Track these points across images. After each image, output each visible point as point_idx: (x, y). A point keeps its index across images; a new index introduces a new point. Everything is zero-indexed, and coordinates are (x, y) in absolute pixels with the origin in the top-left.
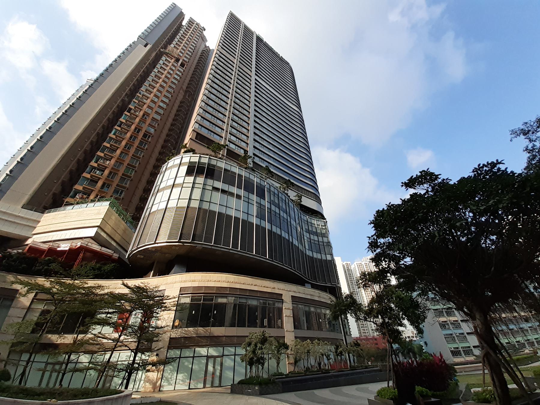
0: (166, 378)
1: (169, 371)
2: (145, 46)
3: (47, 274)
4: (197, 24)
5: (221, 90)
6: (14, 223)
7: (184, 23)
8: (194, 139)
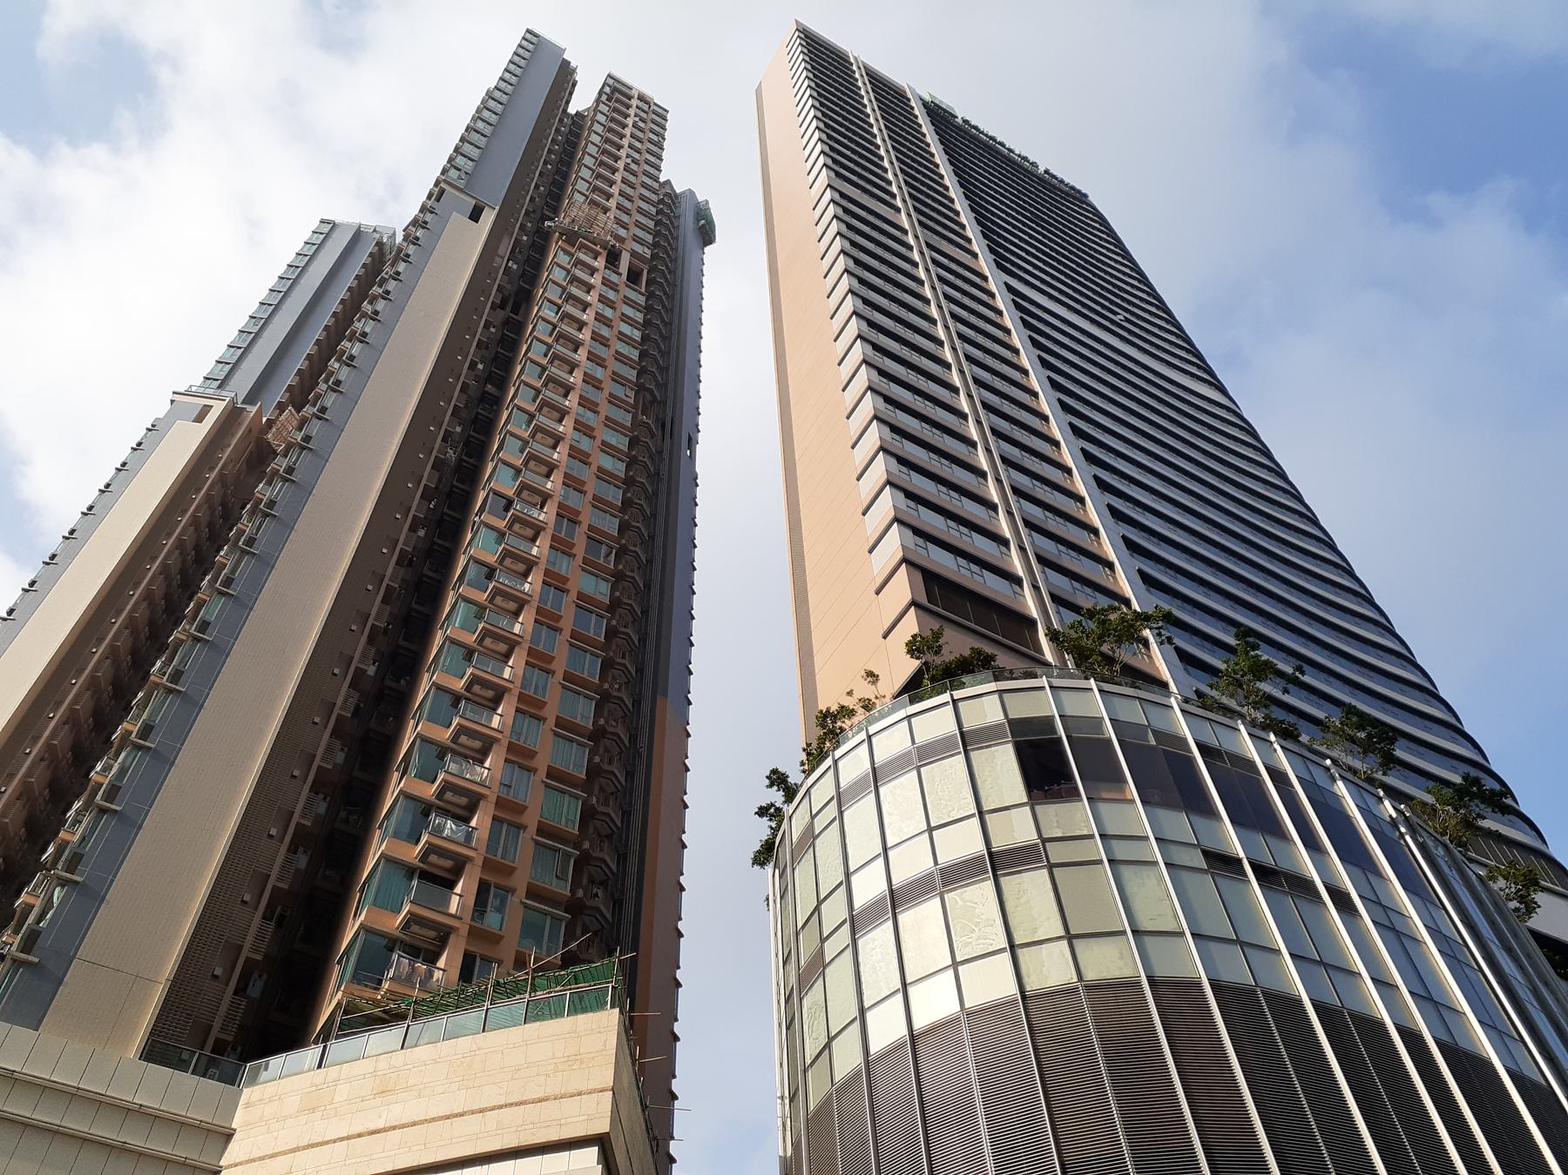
2: (475, 216)
3: (1282, 725)
4: (641, 98)
6: (122, 1150)
7: (581, 100)
8: (924, 600)
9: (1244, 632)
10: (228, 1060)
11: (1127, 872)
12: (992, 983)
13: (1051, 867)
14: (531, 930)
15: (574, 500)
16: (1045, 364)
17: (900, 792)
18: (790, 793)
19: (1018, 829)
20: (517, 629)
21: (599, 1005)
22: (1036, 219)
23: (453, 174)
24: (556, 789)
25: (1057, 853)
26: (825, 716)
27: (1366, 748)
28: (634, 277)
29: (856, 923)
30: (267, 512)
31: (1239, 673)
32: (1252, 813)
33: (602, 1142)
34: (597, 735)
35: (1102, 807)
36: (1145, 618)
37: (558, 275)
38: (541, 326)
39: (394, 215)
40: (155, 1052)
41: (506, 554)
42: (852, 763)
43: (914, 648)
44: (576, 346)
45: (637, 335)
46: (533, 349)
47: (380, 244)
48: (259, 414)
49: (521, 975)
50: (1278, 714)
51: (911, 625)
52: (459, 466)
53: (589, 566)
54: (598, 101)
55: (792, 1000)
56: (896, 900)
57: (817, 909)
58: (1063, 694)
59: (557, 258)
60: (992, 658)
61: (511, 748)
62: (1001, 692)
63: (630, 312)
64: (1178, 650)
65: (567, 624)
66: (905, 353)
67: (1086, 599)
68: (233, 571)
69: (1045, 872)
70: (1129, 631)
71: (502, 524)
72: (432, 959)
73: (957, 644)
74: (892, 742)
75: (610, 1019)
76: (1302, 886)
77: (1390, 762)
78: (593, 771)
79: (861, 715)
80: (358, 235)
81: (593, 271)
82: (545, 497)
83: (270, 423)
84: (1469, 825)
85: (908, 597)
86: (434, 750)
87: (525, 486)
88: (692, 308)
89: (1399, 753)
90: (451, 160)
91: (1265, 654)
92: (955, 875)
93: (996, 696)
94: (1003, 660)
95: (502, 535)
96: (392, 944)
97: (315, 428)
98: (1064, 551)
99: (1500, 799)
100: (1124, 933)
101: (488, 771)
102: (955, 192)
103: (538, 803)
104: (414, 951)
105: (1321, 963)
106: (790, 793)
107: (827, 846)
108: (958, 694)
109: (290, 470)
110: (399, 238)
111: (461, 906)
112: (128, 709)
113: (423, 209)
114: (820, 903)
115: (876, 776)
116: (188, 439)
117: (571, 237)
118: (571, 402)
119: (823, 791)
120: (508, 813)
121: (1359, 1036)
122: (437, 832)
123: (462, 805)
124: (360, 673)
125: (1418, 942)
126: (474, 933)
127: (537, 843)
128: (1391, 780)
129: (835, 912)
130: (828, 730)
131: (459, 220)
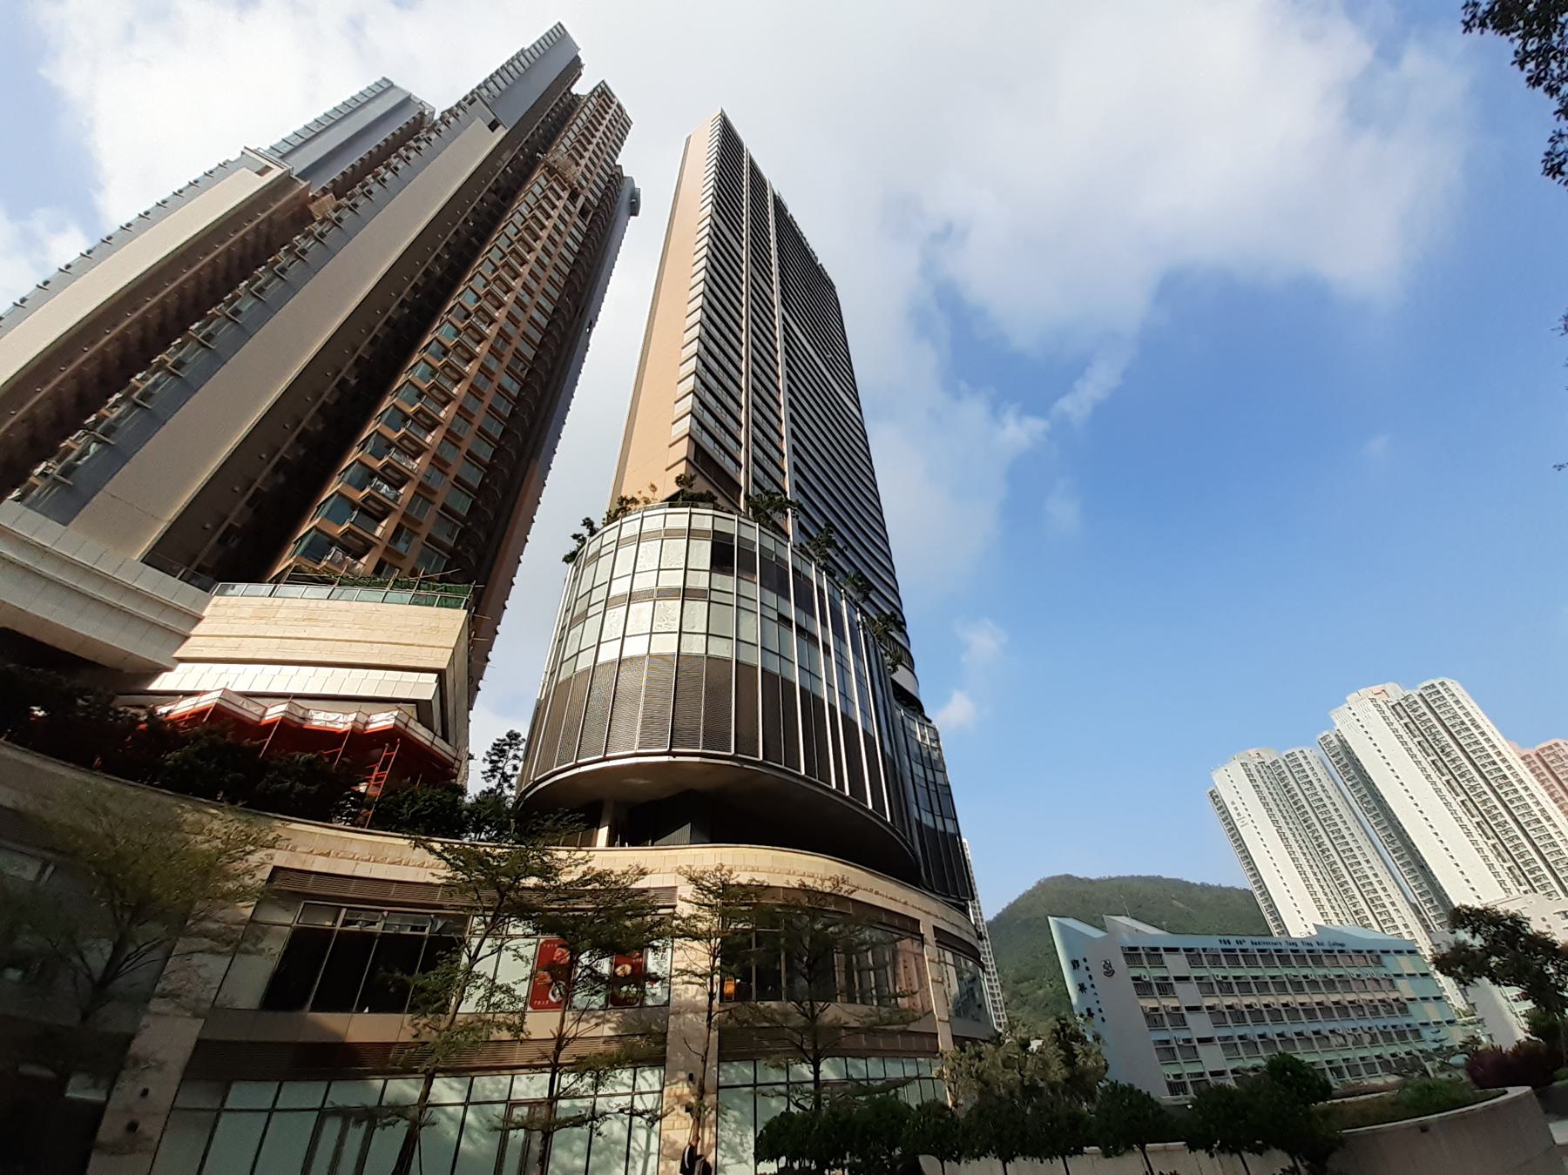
0: (728, 1145)
1: (733, 1126)
2: (493, 126)
4: (619, 106)
5: (726, 331)
6: (120, 610)
7: (582, 88)
9: (829, 524)
10: (206, 579)
11: (743, 613)
12: (666, 645)
14: (424, 558)
15: (510, 329)
16: (788, 364)
17: (650, 549)
18: (593, 532)
19: (700, 581)
20: (455, 391)
21: (458, 607)
23: (484, 91)
25: (715, 596)
26: (623, 499)
27: (859, 590)
28: (583, 213)
29: (608, 603)
31: (819, 543)
32: (805, 604)
33: (441, 674)
34: (490, 467)
36: (790, 502)
38: (517, 216)
39: (439, 96)
40: (151, 559)
41: (458, 344)
42: (630, 527)
43: (679, 481)
44: (536, 238)
46: (511, 226)
47: (422, 114)
48: (308, 188)
49: (412, 579)
50: (830, 564)
51: (681, 469)
52: (440, 280)
53: (509, 371)
54: (592, 93)
55: (565, 630)
56: (631, 597)
59: (538, 181)
61: (435, 457)
65: (487, 400)
66: (721, 357)
67: (768, 485)
68: (267, 284)
70: (782, 507)
71: (461, 326)
72: (358, 557)
73: (700, 486)
74: (654, 522)
75: (462, 614)
76: (814, 639)
77: (866, 598)
79: (642, 505)
80: (408, 100)
81: (559, 198)
82: (493, 321)
83: (314, 198)
84: (886, 631)
86: (385, 443)
87: (480, 309)
88: (613, 247)
90: (486, 82)
91: (834, 536)
92: (665, 594)
94: (720, 501)
96: (332, 541)
97: (347, 215)
98: (765, 461)
99: (901, 625)
101: (416, 465)
103: (444, 491)
104: (347, 550)
106: (593, 532)
107: (605, 563)
109: (322, 235)
110: (437, 117)
111: (384, 533)
112: (168, 346)
113: (458, 105)
115: (640, 538)
116: (247, 185)
117: (551, 171)
118: (524, 270)
119: (611, 536)
120: (424, 492)
121: (812, 703)
122: (377, 488)
123: (397, 479)
124: (343, 382)
128: (864, 606)
129: (598, 595)
130: (622, 507)
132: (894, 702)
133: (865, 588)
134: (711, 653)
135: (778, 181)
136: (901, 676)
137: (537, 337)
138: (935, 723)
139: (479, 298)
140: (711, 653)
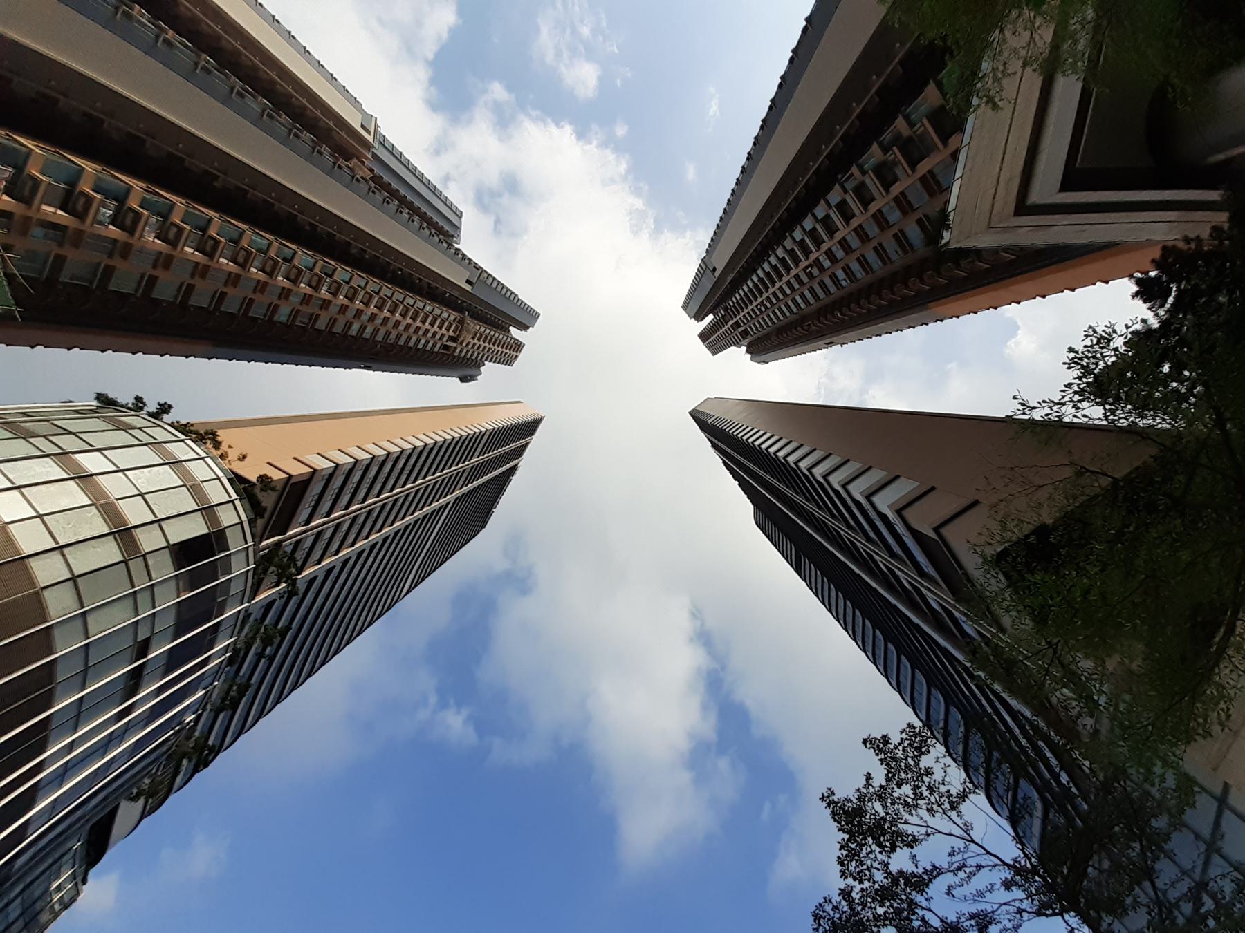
2: (468, 282)
3: (236, 657)
7: (514, 331)
8: (293, 481)
13: (125, 562)
16: (425, 517)
17: (168, 476)
18: (156, 415)
19: (149, 540)
20: (253, 270)
22: (475, 511)
24: (179, 291)
25: (136, 565)
26: (214, 434)
28: (446, 347)
29: (62, 456)
30: (399, 211)
32: (175, 658)
35: (173, 583)
37: (445, 315)
41: (300, 271)
42: (183, 450)
45: (411, 344)
48: (367, 158)
51: (276, 475)
53: (295, 313)
56: (84, 479)
57: (70, 433)
58: (244, 554)
60: (262, 517)
62: (241, 523)
63: (430, 344)
64: (274, 601)
67: (300, 556)
69: (121, 559)
71: (317, 270)
73: (268, 500)
74: (201, 471)
78: (157, 302)
79: (215, 452)
80: (457, 228)
81: (448, 330)
85: (294, 473)
87: (340, 285)
89: (221, 716)
92: (109, 510)
93: (237, 521)
94: (260, 523)
95: (265, 253)
98: (322, 543)
100: (133, 587)
102: (485, 478)
103: (262, 300)
105: (79, 713)
107: (121, 437)
108: (238, 503)
113: (470, 260)
114: (74, 434)
115: (174, 463)
117: (461, 322)
121: (37, 740)
125: (60, 787)
126: (27, 219)
127: (99, 264)
129: (68, 443)
130: (205, 436)
131: (467, 275)
132: (88, 827)
133: (228, 703)
134: (46, 593)
135: (526, 462)
136: (128, 811)
137: (401, 342)
138: (86, 890)
139: (363, 288)
140: (46, 593)
